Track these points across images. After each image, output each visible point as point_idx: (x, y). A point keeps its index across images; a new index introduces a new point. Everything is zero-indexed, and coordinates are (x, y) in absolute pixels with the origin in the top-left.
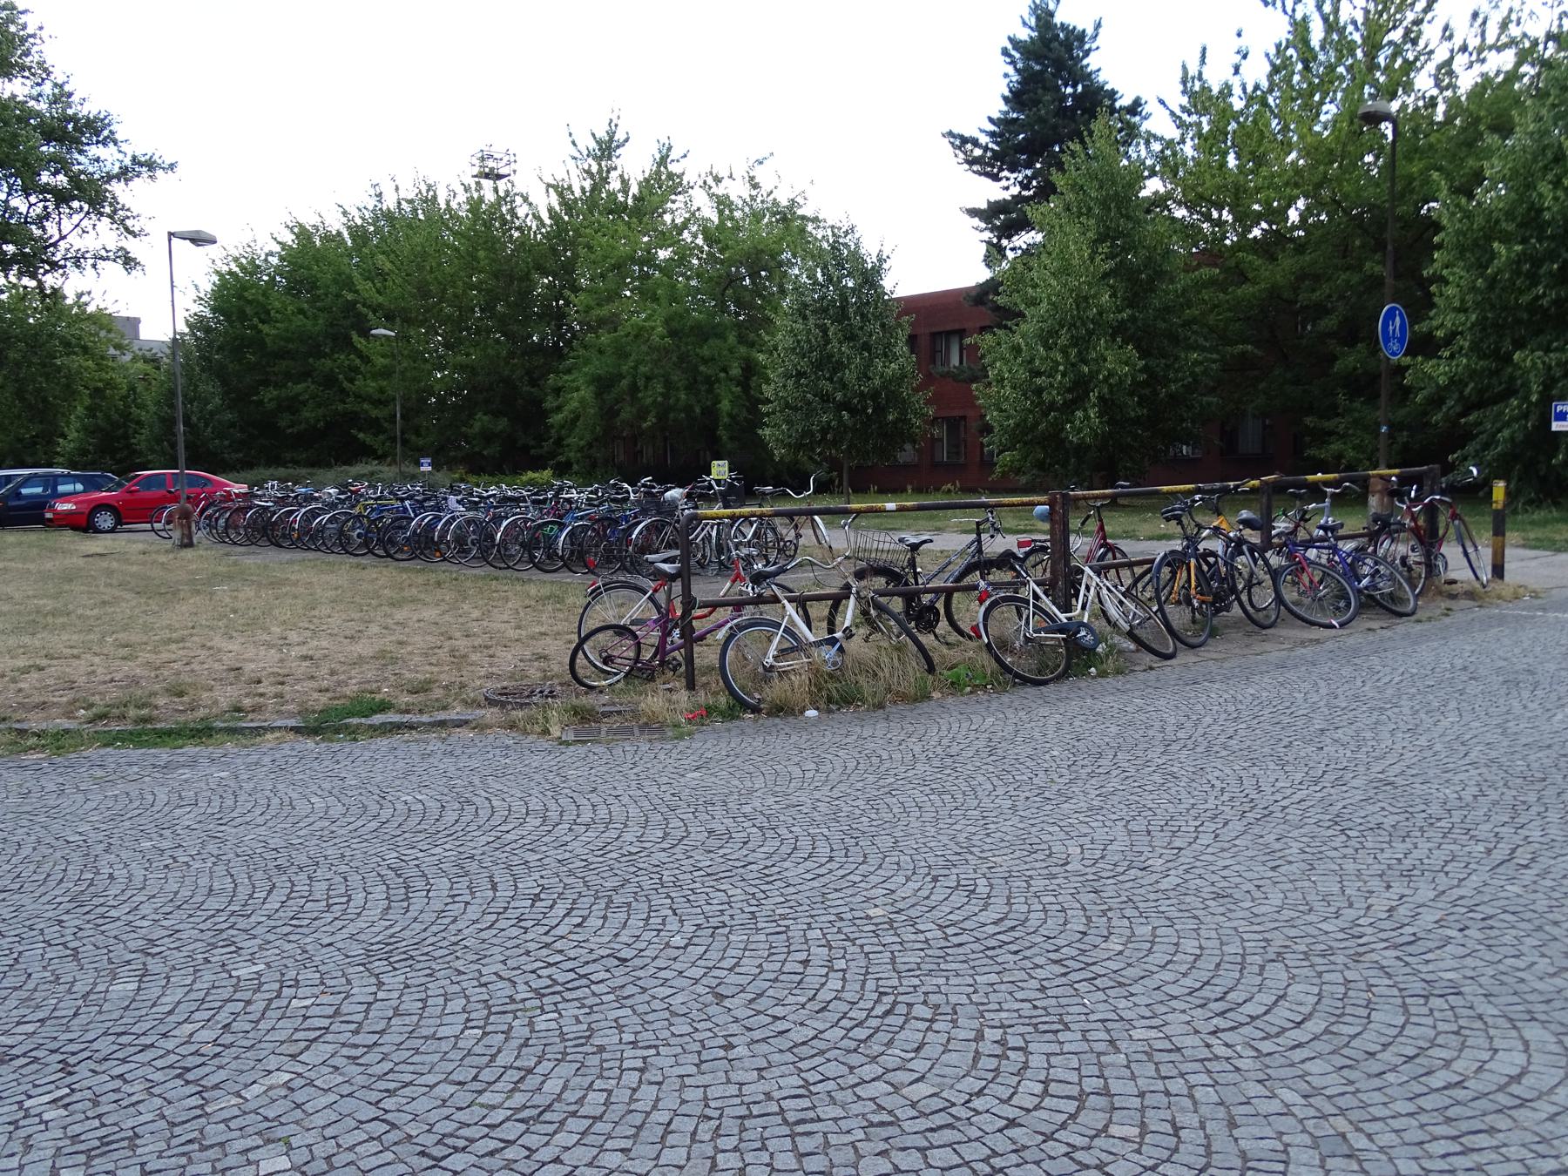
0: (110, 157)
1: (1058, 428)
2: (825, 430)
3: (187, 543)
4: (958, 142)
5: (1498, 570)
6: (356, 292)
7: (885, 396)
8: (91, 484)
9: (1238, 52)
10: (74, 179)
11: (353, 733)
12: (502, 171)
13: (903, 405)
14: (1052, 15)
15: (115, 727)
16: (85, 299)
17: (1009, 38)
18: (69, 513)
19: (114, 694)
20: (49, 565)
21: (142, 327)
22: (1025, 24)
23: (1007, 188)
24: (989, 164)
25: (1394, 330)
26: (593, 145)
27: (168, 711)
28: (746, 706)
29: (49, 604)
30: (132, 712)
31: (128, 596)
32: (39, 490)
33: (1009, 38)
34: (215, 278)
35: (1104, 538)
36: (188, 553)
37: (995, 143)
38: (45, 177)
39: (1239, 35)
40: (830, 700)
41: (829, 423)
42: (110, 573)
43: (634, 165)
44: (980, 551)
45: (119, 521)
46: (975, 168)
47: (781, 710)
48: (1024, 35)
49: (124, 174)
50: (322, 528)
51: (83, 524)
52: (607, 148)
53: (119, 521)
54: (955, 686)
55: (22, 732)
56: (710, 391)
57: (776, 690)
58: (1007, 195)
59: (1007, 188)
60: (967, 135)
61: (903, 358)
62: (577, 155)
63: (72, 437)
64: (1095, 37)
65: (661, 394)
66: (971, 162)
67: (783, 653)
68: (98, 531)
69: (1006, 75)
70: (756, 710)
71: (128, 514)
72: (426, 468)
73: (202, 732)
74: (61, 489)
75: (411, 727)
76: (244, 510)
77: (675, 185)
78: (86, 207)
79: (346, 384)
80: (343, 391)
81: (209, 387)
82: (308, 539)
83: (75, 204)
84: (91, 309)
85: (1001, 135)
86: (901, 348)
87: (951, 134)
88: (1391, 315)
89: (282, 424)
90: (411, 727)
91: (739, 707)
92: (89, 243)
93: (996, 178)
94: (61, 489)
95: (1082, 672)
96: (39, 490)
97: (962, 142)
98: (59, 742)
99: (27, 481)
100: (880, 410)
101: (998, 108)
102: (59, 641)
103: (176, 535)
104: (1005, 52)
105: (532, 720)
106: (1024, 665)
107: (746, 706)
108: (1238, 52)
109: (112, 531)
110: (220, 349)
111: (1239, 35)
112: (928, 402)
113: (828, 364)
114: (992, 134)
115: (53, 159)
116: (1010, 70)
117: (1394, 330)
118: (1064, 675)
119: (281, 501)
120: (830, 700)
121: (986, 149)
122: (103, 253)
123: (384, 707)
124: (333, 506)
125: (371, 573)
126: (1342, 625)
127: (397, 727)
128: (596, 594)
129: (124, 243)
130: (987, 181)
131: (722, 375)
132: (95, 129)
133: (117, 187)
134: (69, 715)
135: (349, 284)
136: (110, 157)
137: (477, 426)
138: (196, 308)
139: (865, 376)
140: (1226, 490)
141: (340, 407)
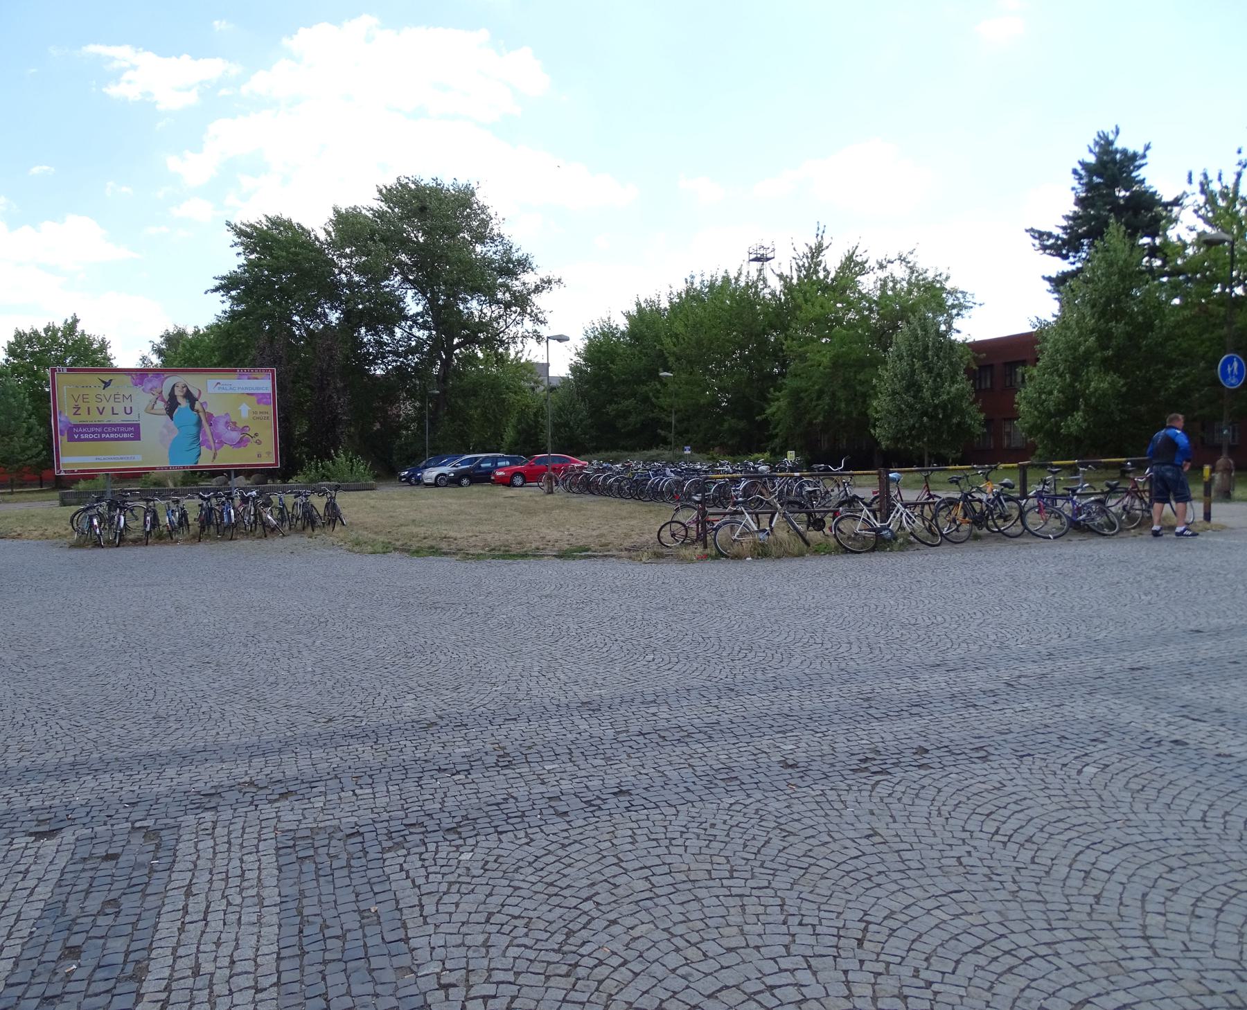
0: (530, 279)
1: (1057, 425)
2: (912, 428)
3: (551, 492)
4: (1037, 235)
5: (1207, 516)
6: (662, 344)
7: (952, 407)
8: (513, 462)
9: (1239, 164)
10: (513, 294)
11: (574, 558)
12: (769, 256)
13: (962, 412)
14: (1111, 143)
15: (497, 553)
16: (520, 355)
17: (1080, 162)
18: (502, 477)
19: (498, 543)
20: (488, 501)
21: (550, 369)
22: (1091, 151)
23: (1074, 263)
24: (1059, 248)
25: (1232, 371)
26: (807, 250)
27: (515, 549)
28: (723, 555)
29: (484, 516)
30: (502, 548)
31: (517, 514)
32: (489, 465)
33: (1080, 162)
34: (587, 341)
35: (928, 491)
36: (549, 497)
37: (1066, 234)
38: (500, 296)
39: (1239, 152)
40: (759, 555)
41: (914, 425)
42: (512, 504)
43: (832, 261)
44: (846, 494)
45: (525, 482)
46: (1048, 251)
47: (738, 557)
48: (1092, 159)
49: (537, 289)
50: (611, 485)
51: (507, 482)
52: (818, 250)
53: (525, 482)
54: (816, 552)
55: (468, 554)
56: (864, 402)
57: (736, 549)
58: (1074, 267)
59: (1074, 263)
60: (1043, 230)
61: (963, 385)
62: (797, 257)
63: (509, 435)
64: (1144, 156)
65: (828, 404)
66: (1044, 248)
67: (741, 535)
68: (515, 486)
69: (1073, 189)
70: (727, 557)
71: (530, 477)
72: (688, 452)
73: (524, 556)
74: (499, 464)
75: (595, 557)
76: (578, 475)
77: (862, 268)
78: (519, 309)
79: (654, 400)
80: (652, 404)
81: (580, 406)
82: (603, 490)
83: (514, 309)
84: (523, 361)
85: (1071, 227)
86: (962, 375)
87: (1032, 230)
88: (1230, 361)
89: (619, 425)
90: (595, 557)
91: (720, 555)
92: (520, 329)
93: (1066, 257)
94: (499, 464)
95: (883, 549)
96: (489, 465)
97: (1040, 235)
98: (478, 557)
99: (485, 460)
100: (947, 417)
101: (1071, 208)
102: (485, 528)
103: (546, 488)
104: (1075, 172)
105: (638, 556)
106: (849, 544)
107: (723, 555)
108: (1239, 164)
109: (521, 486)
110: (587, 382)
111: (1239, 152)
112: (981, 410)
113: (913, 386)
114: (1064, 228)
115: (502, 285)
116: (1075, 184)
117: (1232, 371)
118: (873, 550)
119: (597, 471)
120: (759, 555)
121: (1058, 238)
122: (526, 334)
123: (587, 550)
124: (618, 473)
125: (626, 506)
126: (1055, 538)
127: (590, 557)
128: (677, 510)
129: (537, 327)
130: (1058, 259)
131: (872, 392)
132: (524, 264)
133: (534, 297)
134: (483, 549)
135: (657, 338)
136: (530, 279)
137: (726, 425)
138: (576, 358)
139: (935, 394)
140: (991, 468)
141: (651, 415)
